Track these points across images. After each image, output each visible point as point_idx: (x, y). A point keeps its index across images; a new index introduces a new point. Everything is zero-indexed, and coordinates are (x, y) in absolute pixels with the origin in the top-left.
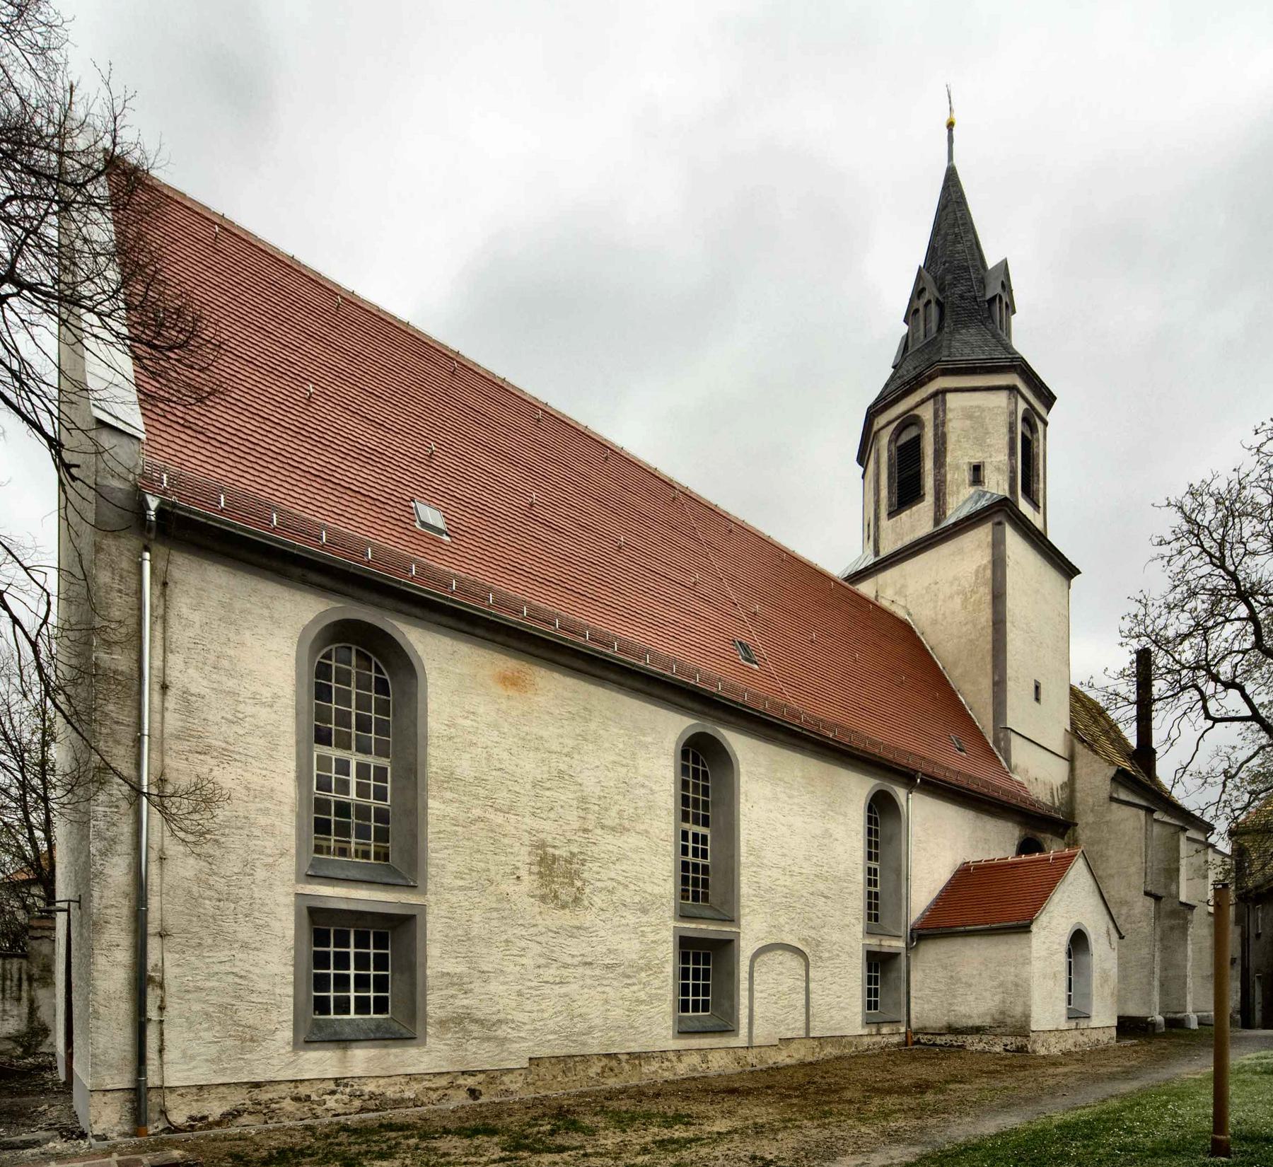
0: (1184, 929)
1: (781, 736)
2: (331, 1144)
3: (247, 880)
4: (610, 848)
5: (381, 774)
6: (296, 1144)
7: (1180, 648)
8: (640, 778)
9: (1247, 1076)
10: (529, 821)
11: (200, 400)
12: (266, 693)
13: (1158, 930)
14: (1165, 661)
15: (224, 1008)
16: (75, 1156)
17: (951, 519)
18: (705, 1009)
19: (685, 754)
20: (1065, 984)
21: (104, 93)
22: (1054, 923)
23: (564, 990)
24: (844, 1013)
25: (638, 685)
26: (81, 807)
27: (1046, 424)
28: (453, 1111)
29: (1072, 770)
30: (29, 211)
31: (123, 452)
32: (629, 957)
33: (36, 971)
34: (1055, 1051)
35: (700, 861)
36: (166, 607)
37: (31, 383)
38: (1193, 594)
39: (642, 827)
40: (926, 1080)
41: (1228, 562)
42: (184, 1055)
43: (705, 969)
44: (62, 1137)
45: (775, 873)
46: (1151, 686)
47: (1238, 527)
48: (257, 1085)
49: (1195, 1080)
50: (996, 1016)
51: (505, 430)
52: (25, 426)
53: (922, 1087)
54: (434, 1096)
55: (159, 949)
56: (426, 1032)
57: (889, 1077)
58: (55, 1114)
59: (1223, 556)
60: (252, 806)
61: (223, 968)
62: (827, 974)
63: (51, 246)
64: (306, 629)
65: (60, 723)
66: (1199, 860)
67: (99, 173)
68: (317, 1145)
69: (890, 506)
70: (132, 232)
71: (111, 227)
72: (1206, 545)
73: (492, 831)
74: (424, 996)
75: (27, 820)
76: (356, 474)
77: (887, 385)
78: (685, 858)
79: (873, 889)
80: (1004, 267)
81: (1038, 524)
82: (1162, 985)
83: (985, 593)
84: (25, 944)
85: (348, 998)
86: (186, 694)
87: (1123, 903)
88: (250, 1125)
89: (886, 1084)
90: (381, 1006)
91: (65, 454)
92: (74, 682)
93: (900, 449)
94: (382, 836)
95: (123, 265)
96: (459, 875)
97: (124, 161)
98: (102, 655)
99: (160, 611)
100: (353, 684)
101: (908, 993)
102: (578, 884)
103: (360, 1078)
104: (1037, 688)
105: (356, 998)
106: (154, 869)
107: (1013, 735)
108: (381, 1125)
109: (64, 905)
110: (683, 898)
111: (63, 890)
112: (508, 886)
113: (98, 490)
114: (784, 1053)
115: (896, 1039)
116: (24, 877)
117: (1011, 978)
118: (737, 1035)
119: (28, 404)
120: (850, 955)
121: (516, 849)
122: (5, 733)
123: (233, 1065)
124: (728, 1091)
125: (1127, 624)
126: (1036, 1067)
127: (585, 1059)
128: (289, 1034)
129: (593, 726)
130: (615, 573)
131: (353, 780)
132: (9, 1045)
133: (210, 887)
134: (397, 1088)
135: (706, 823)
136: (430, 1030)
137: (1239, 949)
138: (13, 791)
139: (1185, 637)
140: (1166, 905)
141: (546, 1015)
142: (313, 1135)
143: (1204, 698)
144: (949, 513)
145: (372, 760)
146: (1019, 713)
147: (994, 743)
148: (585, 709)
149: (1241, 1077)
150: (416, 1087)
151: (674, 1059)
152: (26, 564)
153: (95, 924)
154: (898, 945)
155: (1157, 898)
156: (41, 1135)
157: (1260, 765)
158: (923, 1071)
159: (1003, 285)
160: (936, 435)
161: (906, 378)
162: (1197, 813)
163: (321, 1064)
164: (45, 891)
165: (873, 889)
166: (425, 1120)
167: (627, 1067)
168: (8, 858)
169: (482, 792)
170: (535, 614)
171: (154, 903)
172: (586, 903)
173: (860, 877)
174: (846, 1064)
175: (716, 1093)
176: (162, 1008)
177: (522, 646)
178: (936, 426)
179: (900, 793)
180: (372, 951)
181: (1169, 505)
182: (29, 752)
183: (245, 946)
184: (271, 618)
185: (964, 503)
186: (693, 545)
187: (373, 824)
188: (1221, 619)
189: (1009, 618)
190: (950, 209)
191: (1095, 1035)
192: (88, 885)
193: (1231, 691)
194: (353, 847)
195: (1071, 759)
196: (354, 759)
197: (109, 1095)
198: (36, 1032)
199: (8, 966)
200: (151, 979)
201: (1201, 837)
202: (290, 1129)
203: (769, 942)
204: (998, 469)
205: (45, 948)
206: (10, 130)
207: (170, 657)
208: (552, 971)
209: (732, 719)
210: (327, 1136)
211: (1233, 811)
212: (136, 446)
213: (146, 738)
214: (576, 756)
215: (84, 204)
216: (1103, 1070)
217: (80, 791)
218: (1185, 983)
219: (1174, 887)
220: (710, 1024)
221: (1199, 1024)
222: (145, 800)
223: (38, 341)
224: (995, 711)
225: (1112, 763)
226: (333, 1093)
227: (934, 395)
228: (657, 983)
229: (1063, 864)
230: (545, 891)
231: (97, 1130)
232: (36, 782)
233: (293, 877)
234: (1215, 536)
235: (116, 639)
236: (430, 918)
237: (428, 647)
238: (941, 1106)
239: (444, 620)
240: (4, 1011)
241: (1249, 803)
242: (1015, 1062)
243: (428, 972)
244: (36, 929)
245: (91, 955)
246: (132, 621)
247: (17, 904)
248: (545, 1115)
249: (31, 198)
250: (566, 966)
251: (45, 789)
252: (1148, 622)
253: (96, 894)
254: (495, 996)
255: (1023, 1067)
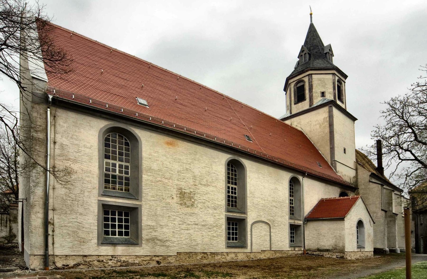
0: (394, 221)
1: (260, 161)
2: (110, 276)
3: (82, 195)
4: (204, 190)
5: (127, 167)
6: (99, 276)
7: (390, 140)
8: (213, 171)
9: (418, 269)
10: (176, 182)
11: (66, 73)
12: (88, 145)
13: (386, 221)
14: (386, 143)
15: (74, 232)
16: (24, 275)
17: (315, 105)
18: (236, 240)
19: (228, 165)
20: (356, 237)
21: (36, 5)
22: (352, 218)
23: (188, 232)
24: (283, 243)
25: (212, 146)
26: (27, 173)
27: (345, 82)
28: (151, 268)
29: (357, 173)
30: (11, 30)
31: (41, 84)
32: (210, 223)
33: (12, 218)
34: (353, 258)
35: (234, 195)
36: (55, 122)
37: (11, 68)
38: (394, 126)
39: (214, 185)
40: (311, 266)
41: (405, 118)
42: (61, 245)
43: (236, 228)
44: (20, 269)
45: (259, 200)
46: (381, 150)
47: (407, 109)
48: (85, 256)
49: (400, 270)
50: (334, 246)
51: (167, 81)
52: (9, 78)
53: (309, 268)
54: (145, 263)
55: (52, 214)
56: (142, 243)
57: (298, 264)
58: (18, 261)
59: (403, 116)
60: (84, 175)
61: (73, 220)
62: (277, 231)
63: (18, 38)
64: (101, 129)
65: (21, 151)
66: (399, 200)
67: (34, 22)
68: (106, 276)
69: (295, 101)
70: (44, 35)
71: (37, 34)
72: (398, 113)
73: (164, 184)
74: (141, 231)
75: (10, 176)
76: (117, 90)
77: (293, 72)
78: (229, 194)
79: (292, 205)
80: (330, 46)
81: (343, 106)
82: (388, 239)
83: (327, 124)
84: (8, 210)
85: (116, 231)
86: (62, 145)
87: (374, 212)
88: (83, 268)
89: (297, 267)
90: (127, 234)
91: (22, 85)
92: (25, 141)
93: (297, 88)
94: (127, 184)
95: (41, 42)
96: (153, 196)
97: (42, 19)
98: (34, 134)
99: (53, 123)
100: (117, 143)
101: (304, 238)
102: (193, 200)
103: (120, 256)
104: (345, 150)
105: (118, 231)
106: (51, 192)
107: (337, 163)
108: (127, 271)
109: (22, 200)
110: (228, 206)
111: (21, 196)
112: (169, 200)
113: (32, 93)
114: (263, 255)
115: (300, 252)
116: (9, 192)
117: (338, 234)
118: (247, 248)
119: (10, 73)
120: (284, 225)
121: (172, 190)
122: (3, 153)
123: (77, 249)
124: (245, 266)
125: (373, 133)
126: (347, 263)
127: (196, 253)
128: (96, 241)
129: (198, 156)
130: (204, 117)
131: (117, 169)
132: (3, 240)
133: (70, 197)
134: (132, 260)
135: (236, 184)
136: (143, 242)
137: (414, 228)
138: (6, 169)
139: (392, 137)
140: (389, 214)
141: (182, 239)
142: (104, 273)
143: (398, 153)
144: (314, 104)
145: (124, 164)
146: (339, 156)
147: (331, 164)
148: (195, 152)
149: (416, 269)
150: (139, 259)
151: (226, 255)
152: (10, 111)
153: (31, 206)
154: (301, 223)
155: (386, 212)
156: (13, 268)
157: (419, 173)
158: (310, 263)
159: (329, 50)
160: (309, 85)
161: (299, 71)
162: (398, 186)
163: (106, 251)
164: (15, 196)
165: (292, 205)
166: (142, 270)
167: (210, 257)
168: (3, 187)
169: (161, 173)
170: (177, 126)
171: (51, 201)
172: (195, 206)
173: (287, 202)
174: (284, 260)
175: (240, 267)
176: (53, 231)
177: (173, 135)
178: (309, 83)
179: (300, 178)
180: (123, 217)
181: (385, 103)
182: (11, 158)
183: (81, 214)
184: (90, 126)
185: (319, 101)
186: (230, 110)
187: (124, 181)
188: (403, 133)
189: (335, 131)
190: (312, 32)
191: (366, 254)
192: (29, 195)
193: (407, 152)
194: (117, 187)
195: (356, 170)
196: (118, 163)
197: (36, 256)
198: (12, 236)
199: (3, 217)
200: (50, 223)
201: (399, 194)
202: (97, 270)
203: (257, 220)
204: (330, 93)
205: (15, 212)
206: (6, 12)
207: (57, 135)
208: (184, 226)
209: (244, 156)
210: (109, 274)
211: (410, 186)
212: (45, 83)
213: (49, 156)
214: (192, 164)
215: (28, 29)
216: (369, 265)
217: (27, 169)
218: (395, 238)
219: (391, 208)
220: (238, 245)
221: (401, 251)
222: (48, 172)
223: (14, 59)
224: (331, 156)
225: (370, 171)
226: (111, 260)
227: (309, 75)
228: (219, 231)
229: (354, 201)
230: (181, 202)
231: (32, 267)
232: (13, 166)
233: (97, 195)
234: (400, 111)
235: (39, 130)
236: (143, 208)
237: (140, 134)
238: (316, 275)
239: (147, 127)
240: (1, 229)
241: (416, 184)
242: (340, 261)
243: (143, 224)
244: (12, 206)
245: (30, 215)
246: (44, 126)
247: (6, 199)
248: (182, 271)
249: (12, 27)
250: (189, 225)
251: (16, 168)
252: (380, 133)
253: (32, 197)
254: (165, 232)
255: (343, 263)
